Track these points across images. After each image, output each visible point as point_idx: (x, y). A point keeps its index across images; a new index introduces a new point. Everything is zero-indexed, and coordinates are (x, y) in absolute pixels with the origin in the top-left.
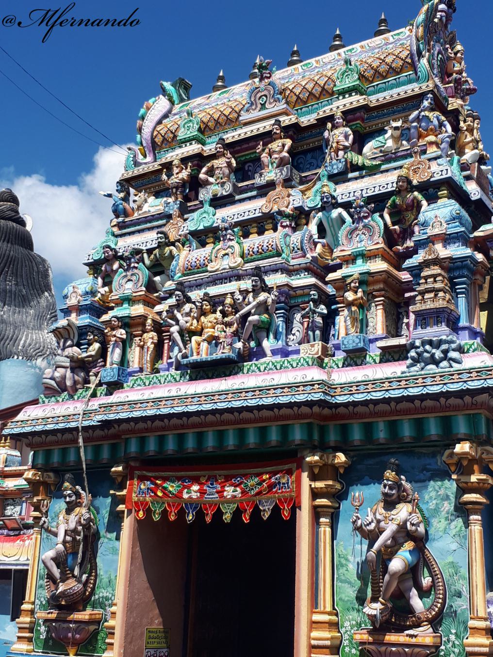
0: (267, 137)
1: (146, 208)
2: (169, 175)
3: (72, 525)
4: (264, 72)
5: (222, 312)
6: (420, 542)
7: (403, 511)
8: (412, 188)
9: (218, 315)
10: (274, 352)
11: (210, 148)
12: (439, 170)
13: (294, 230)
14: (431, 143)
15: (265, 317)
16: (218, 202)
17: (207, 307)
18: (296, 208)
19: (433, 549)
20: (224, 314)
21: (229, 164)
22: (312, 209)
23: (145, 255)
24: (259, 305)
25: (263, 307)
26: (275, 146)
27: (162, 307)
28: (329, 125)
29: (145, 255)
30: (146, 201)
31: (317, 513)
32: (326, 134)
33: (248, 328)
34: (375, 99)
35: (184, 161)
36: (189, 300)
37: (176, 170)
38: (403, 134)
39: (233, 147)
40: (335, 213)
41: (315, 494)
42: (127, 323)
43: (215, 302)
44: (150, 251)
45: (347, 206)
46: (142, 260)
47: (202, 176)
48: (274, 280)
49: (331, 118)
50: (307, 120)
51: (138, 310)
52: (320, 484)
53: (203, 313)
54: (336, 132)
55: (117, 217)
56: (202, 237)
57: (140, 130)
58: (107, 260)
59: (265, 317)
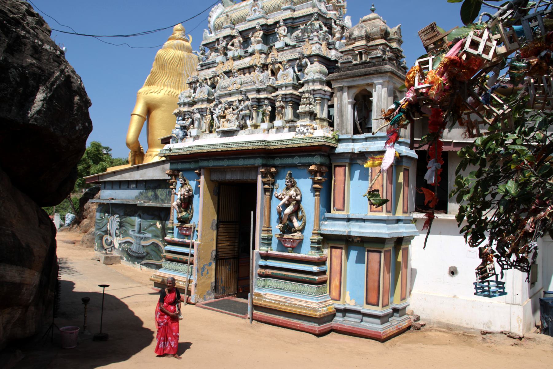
0: (253, 29)
1: (211, 58)
2: (218, 45)
3: (183, 193)
4: (196, 21)
5: (233, 108)
6: (298, 202)
7: (292, 192)
8: (304, 57)
9: (231, 110)
10: (251, 126)
11: (234, 33)
12: (314, 49)
13: (262, 72)
14: (315, 36)
15: (248, 112)
16: (234, 59)
17: (227, 106)
18: (262, 64)
19: (302, 205)
20: (233, 110)
21: (239, 41)
22: (269, 64)
23: (208, 80)
24: (245, 107)
25: (247, 107)
26: (256, 34)
27: (212, 105)
28: (278, 25)
29: (208, 80)
30: (210, 54)
31: (265, 190)
32: (276, 30)
33: (241, 117)
34: (296, 14)
35: (224, 38)
36: (221, 103)
37: (221, 42)
38: (304, 31)
39: (241, 33)
40: (277, 66)
41: (264, 184)
42: (201, 111)
43: (230, 104)
44: (210, 79)
45: (280, 63)
46: (207, 83)
47: (229, 47)
48: (252, 95)
49: (278, 22)
50: (270, 22)
51: (205, 105)
52: (265, 180)
53: (226, 109)
54: (280, 28)
55: (200, 61)
56: (228, 73)
57: (209, 22)
58: (195, 83)
59: (248, 112)
